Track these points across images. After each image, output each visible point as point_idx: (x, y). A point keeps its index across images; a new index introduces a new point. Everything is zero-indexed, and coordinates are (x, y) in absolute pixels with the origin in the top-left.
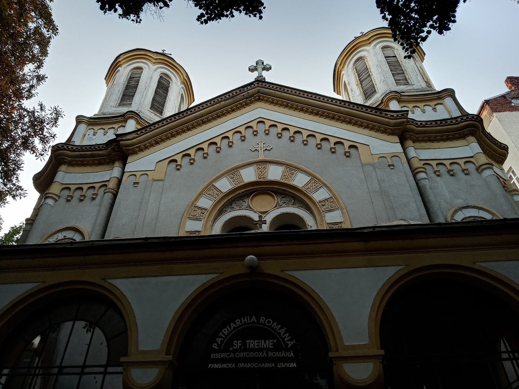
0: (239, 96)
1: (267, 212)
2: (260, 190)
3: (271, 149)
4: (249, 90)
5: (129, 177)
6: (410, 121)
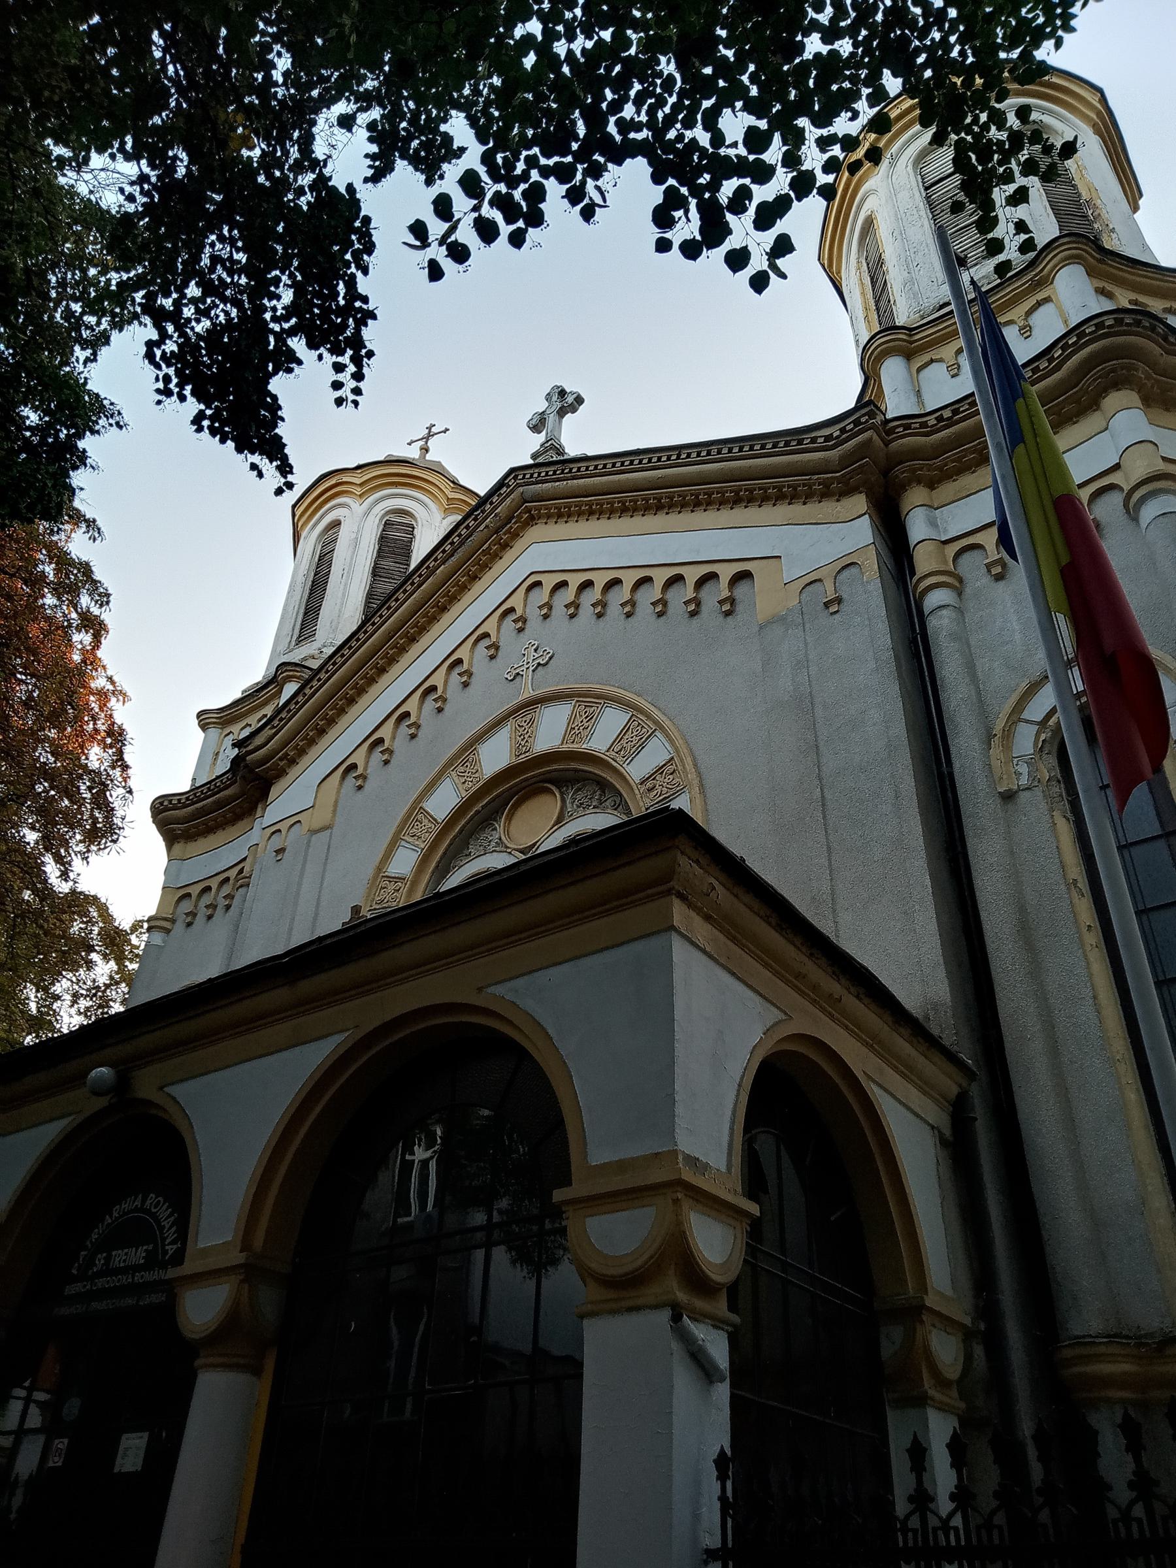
0: (475, 534)
2: (524, 788)
3: (551, 658)
4: (496, 508)
5: (270, 838)
6: (898, 426)
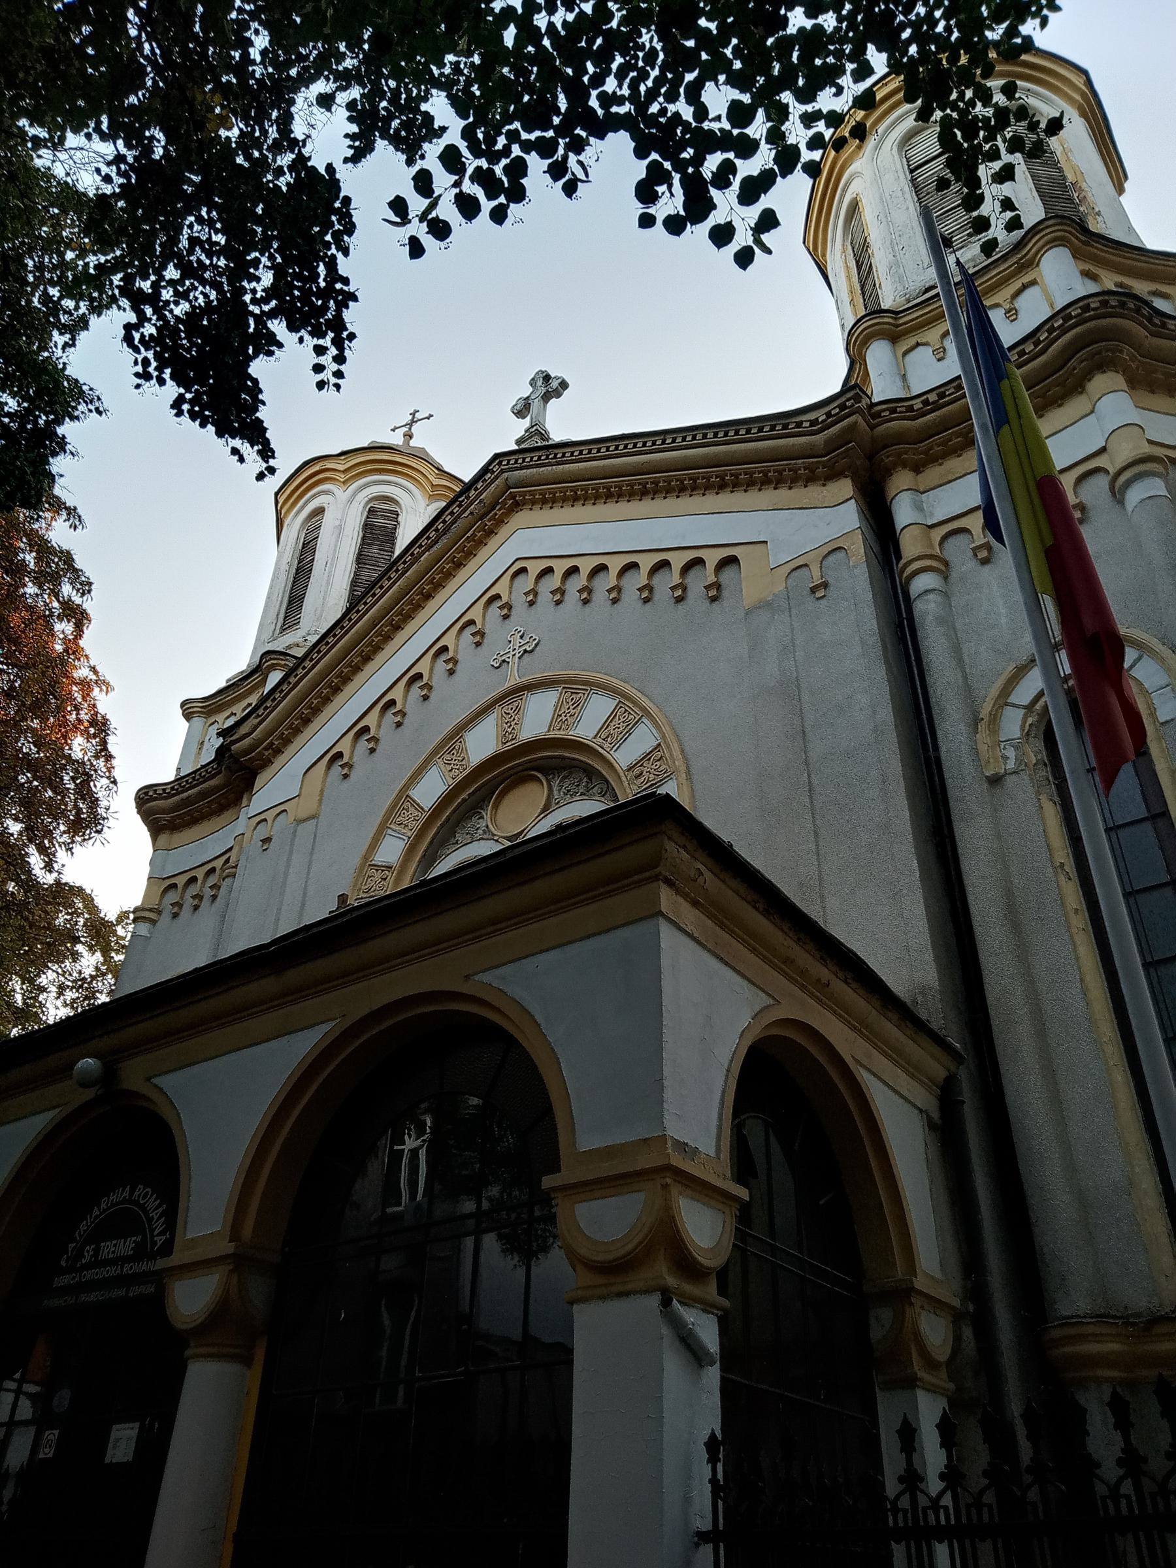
2: (511, 775)
3: (536, 645)
4: (481, 494)
6: (884, 410)
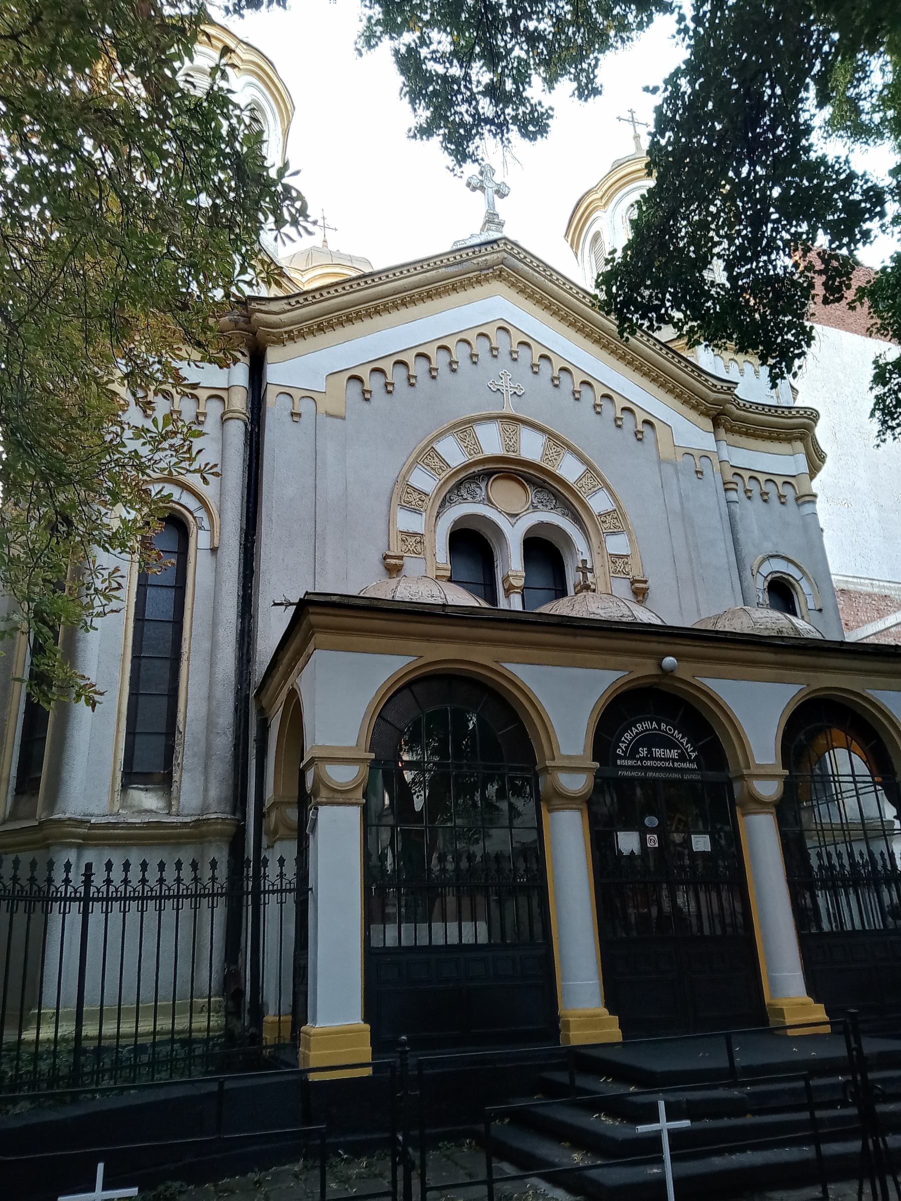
1: (492, 504)
